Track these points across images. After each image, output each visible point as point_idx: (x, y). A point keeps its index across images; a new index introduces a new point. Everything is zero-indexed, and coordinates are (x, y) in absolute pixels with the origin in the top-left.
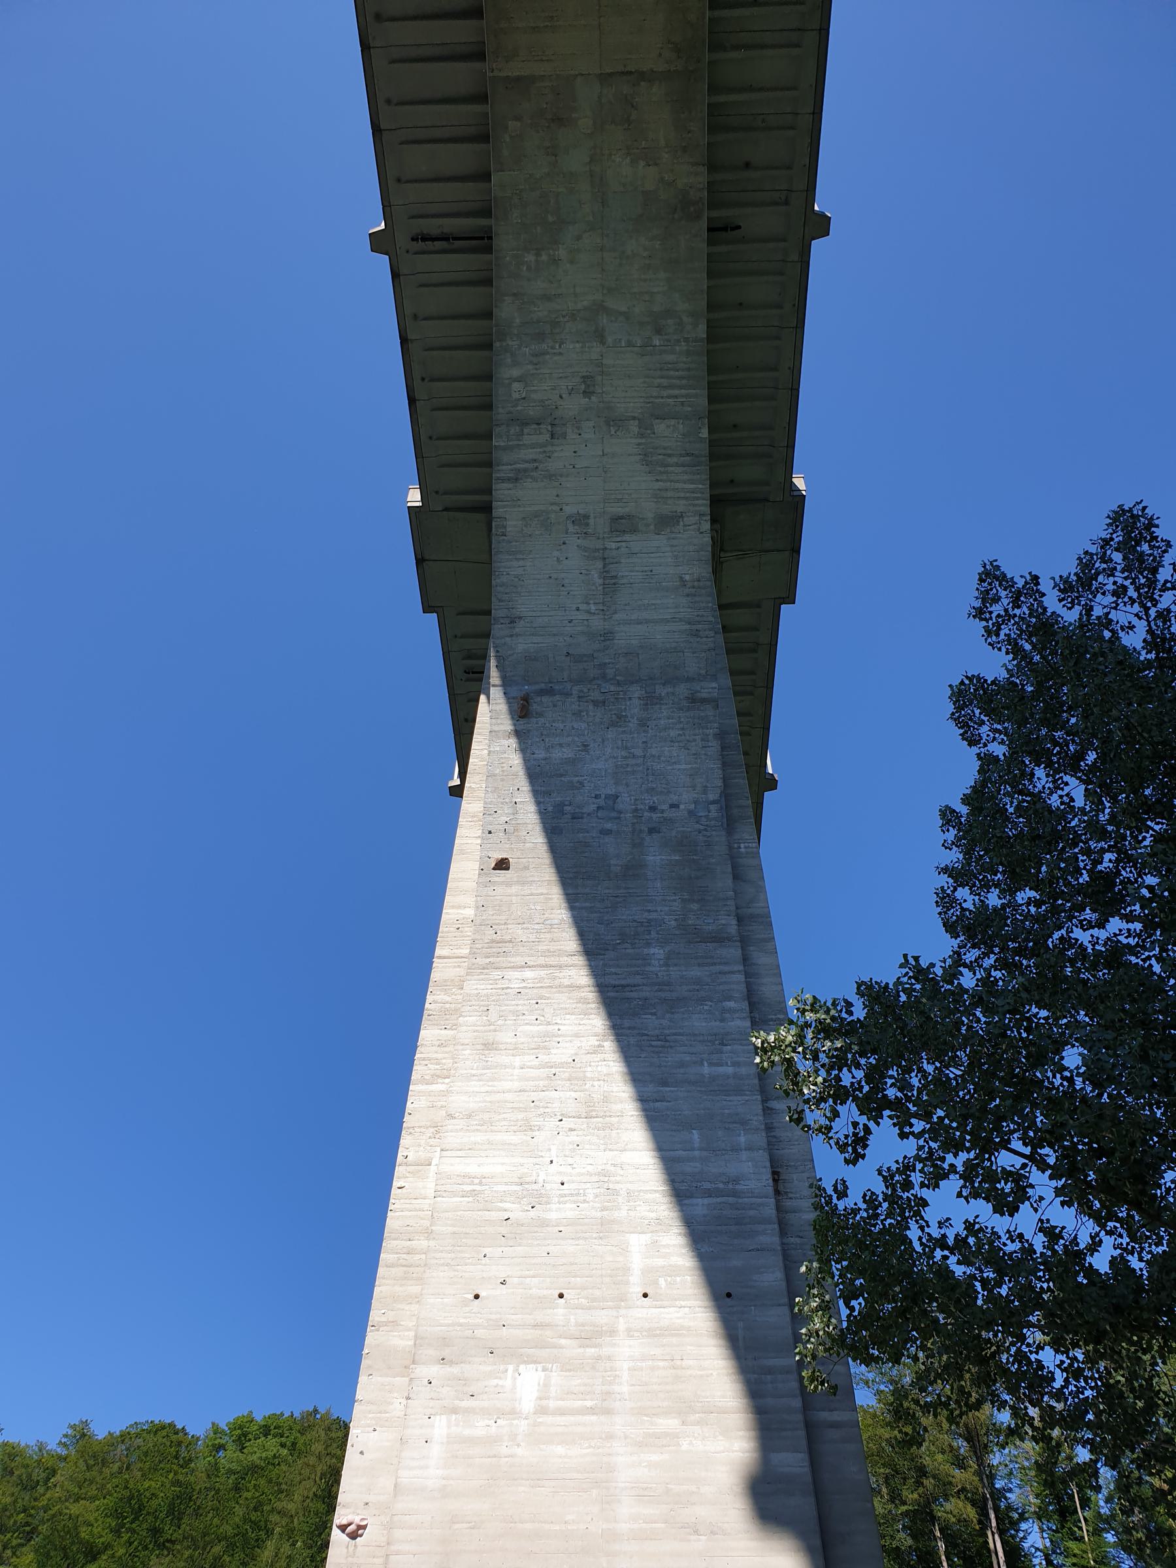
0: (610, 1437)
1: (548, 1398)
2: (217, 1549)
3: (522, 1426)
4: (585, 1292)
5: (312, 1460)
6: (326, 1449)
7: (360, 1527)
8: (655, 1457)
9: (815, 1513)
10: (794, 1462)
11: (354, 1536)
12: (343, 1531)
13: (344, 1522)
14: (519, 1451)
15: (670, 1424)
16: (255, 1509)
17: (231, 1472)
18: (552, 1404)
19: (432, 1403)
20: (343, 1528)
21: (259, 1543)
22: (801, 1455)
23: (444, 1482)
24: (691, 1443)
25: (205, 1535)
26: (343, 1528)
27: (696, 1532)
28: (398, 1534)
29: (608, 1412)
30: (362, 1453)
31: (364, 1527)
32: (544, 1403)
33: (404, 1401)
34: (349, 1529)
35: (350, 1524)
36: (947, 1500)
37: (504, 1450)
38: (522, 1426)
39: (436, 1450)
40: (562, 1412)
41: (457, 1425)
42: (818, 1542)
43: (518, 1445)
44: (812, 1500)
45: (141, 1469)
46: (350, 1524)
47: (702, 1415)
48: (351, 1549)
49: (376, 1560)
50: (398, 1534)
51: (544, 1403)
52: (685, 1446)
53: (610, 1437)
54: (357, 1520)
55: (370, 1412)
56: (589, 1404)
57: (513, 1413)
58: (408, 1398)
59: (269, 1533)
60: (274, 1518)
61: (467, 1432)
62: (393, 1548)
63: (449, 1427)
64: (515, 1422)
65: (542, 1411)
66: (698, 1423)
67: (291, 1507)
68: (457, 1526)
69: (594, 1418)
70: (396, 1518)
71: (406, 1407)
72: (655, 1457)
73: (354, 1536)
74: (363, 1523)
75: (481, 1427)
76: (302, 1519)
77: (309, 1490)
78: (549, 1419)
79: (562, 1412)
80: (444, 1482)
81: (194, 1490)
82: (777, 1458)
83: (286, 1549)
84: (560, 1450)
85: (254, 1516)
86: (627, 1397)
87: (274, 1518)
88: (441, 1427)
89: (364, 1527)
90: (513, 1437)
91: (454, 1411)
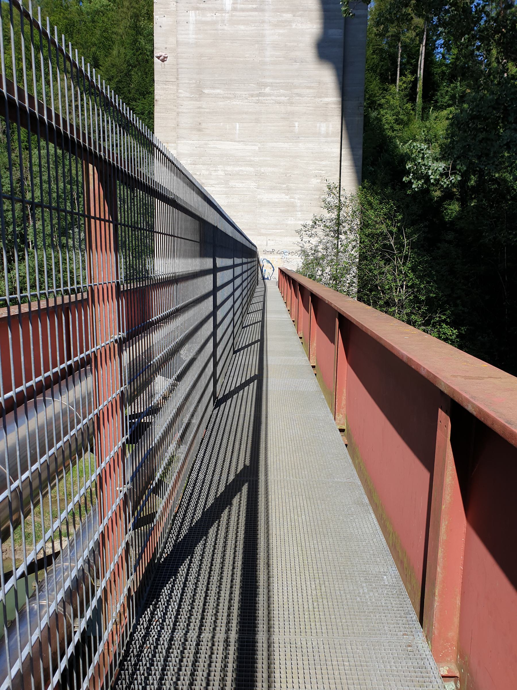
0: (263, 22)
1: (237, 4)
2: (93, 49)
3: (227, 16)
4: (298, 98)
5: (125, 10)
6: (130, 4)
7: (165, 57)
8: (281, 31)
9: (343, 55)
10: (337, 33)
11: (163, 61)
12: (159, 59)
13: (158, 55)
14: (226, 28)
15: (288, 16)
16: (104, 31)
17: (88, 13)
18: (239, 6)
19: (187, 5)
20: (158, 58)
21: (110, 48)
22: (340, 31)
23: (196, 40)
24: (296, 25)
25: (86, 43)
26: (158, 58)
27: (296, 62)
28: (181, 61)
29: (262, 10)
30: (160, 26)
31: (167, 57)
32: (235, 6)
33: (175, 3)
34: (161, 58)
35: (161, 56)
36: (381, 121)
37: (219, 27)
38: (227, 16)
39: (191, 27)
40: (243, 10)
41: (199, 16)
42: (342, 66)
43: (225, 25)
44: (342, 49)
45: (47, 11)
46: (161, 56)
47: (302, 12)
48: (163, 66)
49: (173, 70)
50: (181, 61)
51: (235, 6)
52: (294, 26)
53: (263, 22)
54: (163, 54)
55: (161, 8)
56: (254, 6)
57: (222, 10)
58: (177, 2)
59: (113, 43)
60: (114, 36)
61: (204, 19)
62: (179, 66)
63: (196, 16)
64: (224, 14)
65: (234, 9)
66: (300, 16)
67: (120, 31)
68: (203, 58)
69: (256, 13)
70: (179, 55)
71: (176, 6)
72: (281, 31)
73: (163, 61)
74: (166, 56)
75: (209, 17)
76: (126, 36)
77: (126, 23)
78: (238, 13)
79: (243, 10)
80: (196, 40)
81: (74, 22)
82: (331, 31)
83: (122, 50)
84: (242, 27)
85: (105, 34)
86: (271, 3)
87: (114, 36)
88: (192, 16)
89: (167, 57)
90: (223, 21)
91: (197, 9)
